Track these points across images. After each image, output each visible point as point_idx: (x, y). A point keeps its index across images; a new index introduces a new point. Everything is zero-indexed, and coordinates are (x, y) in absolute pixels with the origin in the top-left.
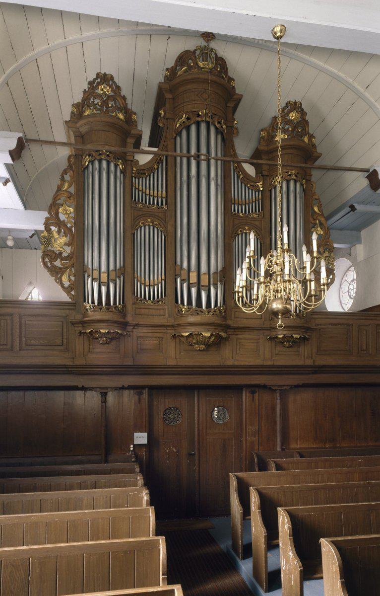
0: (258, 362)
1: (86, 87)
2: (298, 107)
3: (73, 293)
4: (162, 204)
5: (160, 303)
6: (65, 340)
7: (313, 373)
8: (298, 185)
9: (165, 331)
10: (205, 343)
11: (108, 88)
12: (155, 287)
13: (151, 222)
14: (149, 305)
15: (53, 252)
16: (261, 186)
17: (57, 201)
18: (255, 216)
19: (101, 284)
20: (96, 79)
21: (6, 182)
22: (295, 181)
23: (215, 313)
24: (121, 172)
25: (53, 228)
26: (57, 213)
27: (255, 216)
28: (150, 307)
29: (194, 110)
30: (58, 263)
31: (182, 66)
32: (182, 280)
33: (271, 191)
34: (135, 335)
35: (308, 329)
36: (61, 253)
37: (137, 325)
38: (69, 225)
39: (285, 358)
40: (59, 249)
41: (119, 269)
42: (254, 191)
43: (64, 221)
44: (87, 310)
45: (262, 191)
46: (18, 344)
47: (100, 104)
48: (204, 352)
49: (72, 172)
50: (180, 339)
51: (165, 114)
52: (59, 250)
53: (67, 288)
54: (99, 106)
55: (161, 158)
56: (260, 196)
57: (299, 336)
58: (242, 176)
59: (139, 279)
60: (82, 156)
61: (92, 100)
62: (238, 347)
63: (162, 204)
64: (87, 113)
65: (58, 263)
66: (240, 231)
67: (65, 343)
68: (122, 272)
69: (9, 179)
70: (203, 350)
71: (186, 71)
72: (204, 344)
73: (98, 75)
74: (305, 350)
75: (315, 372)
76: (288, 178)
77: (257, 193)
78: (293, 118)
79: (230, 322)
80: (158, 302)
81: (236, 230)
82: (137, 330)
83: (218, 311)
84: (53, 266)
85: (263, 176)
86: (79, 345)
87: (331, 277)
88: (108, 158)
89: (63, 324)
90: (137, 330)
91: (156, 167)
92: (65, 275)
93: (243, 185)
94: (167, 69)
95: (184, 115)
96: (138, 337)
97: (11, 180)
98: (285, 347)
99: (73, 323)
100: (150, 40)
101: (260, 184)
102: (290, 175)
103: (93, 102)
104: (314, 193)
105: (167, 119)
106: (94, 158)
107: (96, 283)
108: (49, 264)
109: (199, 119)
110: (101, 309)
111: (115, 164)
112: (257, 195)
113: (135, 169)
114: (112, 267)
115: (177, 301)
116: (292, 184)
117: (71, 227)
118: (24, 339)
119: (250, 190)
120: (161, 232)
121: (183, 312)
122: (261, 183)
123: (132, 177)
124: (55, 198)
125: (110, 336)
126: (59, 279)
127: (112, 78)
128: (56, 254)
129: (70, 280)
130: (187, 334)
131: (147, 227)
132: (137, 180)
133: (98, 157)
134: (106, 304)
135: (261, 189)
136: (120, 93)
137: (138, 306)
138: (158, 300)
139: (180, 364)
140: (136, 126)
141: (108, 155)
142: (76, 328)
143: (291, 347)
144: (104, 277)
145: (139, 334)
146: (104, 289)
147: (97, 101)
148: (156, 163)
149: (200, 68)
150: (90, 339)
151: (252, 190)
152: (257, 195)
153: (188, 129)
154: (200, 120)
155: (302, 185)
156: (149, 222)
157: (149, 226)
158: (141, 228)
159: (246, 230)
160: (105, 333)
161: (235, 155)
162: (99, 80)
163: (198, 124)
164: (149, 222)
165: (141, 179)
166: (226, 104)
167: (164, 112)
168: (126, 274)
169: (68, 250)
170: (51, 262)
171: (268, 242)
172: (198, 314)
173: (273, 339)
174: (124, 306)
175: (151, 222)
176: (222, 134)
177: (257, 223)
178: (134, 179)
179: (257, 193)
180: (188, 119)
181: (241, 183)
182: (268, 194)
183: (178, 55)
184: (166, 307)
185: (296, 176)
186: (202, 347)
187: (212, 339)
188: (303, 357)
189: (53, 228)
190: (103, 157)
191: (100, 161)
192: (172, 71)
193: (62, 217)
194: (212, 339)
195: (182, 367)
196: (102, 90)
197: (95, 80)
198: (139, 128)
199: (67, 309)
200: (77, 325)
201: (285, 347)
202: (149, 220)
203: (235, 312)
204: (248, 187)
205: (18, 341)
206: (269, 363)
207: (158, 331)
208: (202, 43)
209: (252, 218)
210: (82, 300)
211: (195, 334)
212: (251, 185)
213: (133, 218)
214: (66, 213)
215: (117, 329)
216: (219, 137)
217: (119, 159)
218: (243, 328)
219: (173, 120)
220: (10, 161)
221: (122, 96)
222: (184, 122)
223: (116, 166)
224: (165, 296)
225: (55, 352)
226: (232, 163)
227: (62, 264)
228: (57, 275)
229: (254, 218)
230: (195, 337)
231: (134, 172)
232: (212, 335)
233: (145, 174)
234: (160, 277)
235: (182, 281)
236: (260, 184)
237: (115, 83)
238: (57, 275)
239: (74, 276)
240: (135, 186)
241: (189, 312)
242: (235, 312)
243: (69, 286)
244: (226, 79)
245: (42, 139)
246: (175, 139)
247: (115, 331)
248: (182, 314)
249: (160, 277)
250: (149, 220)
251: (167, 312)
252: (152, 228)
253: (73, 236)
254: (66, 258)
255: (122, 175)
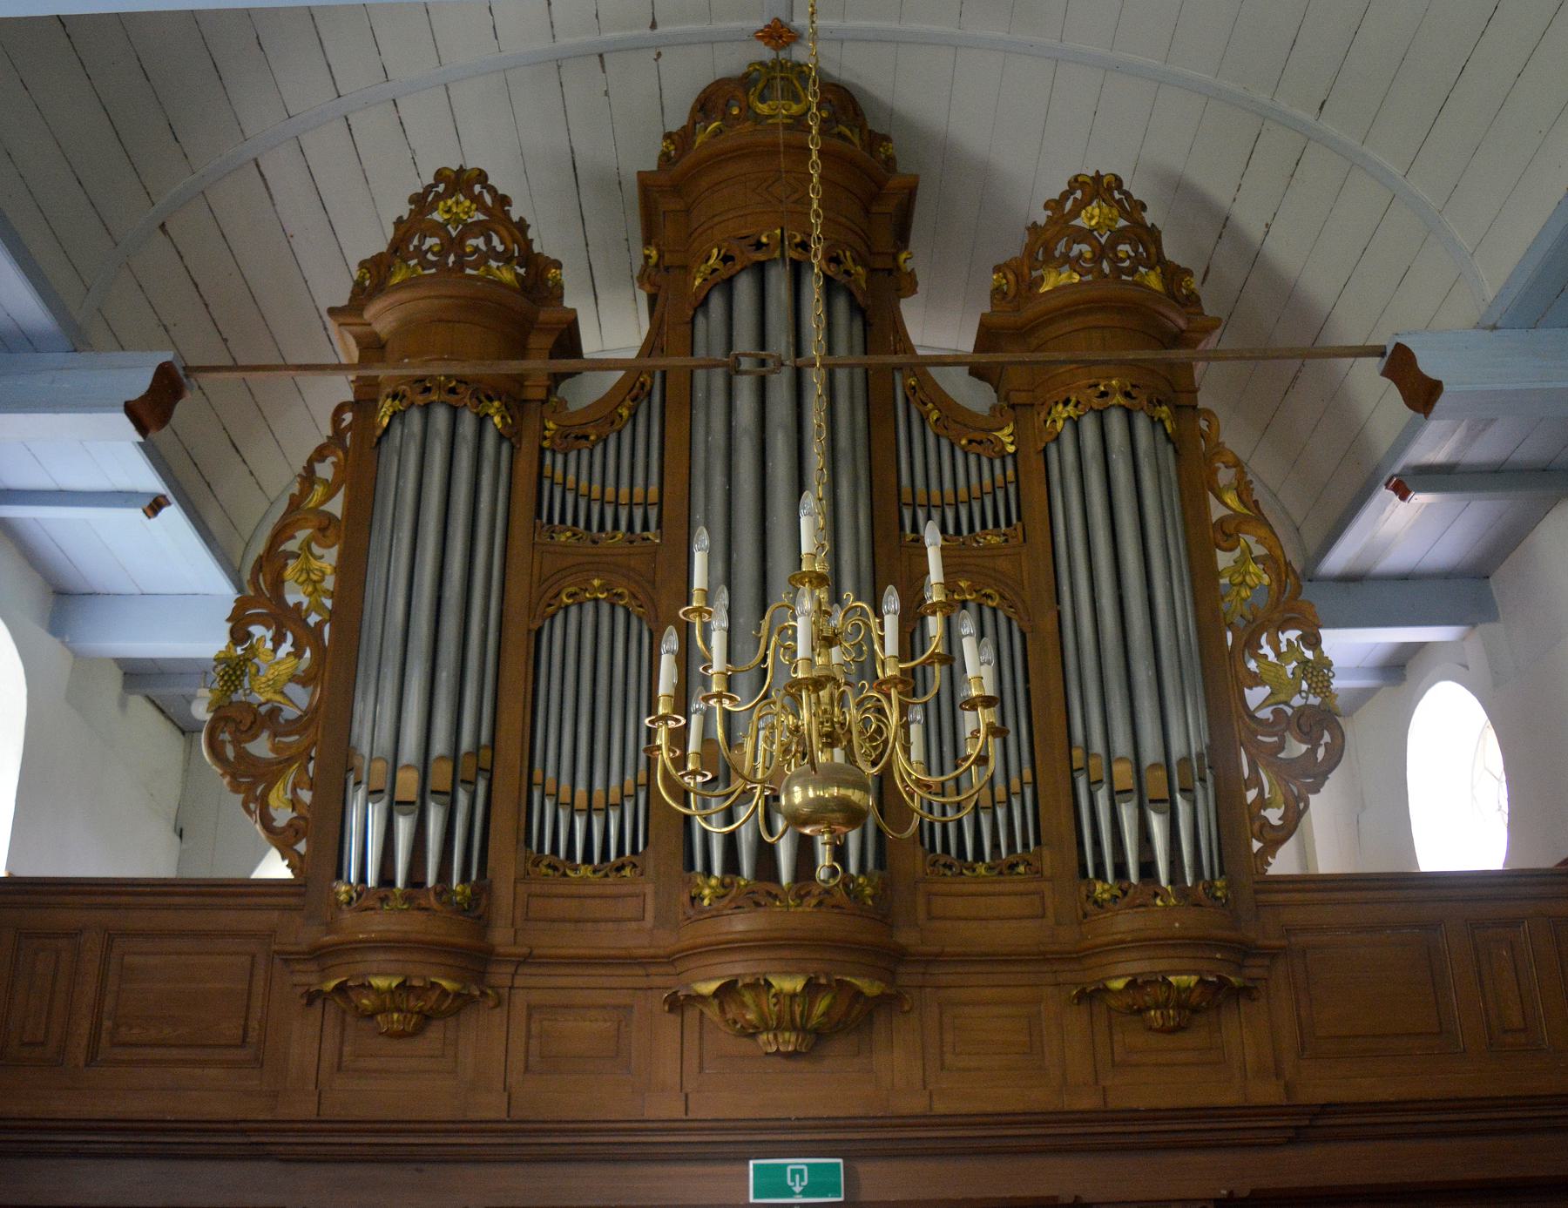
0: (1038, 1097)
1: (404, 210)
2: (1109, 189)
3: (302, 847)
4: (646, 527)
5: (627, 872)
6: (254, 1024)
7: (1291, 1141)
8: (1142, 424)
9: (642, 982)
10: (793, 1020)
11: (467, 203)
12: (595, 818)
13: (602, 589)
14: (584, 881)
15: (248, 706)
16: (1010, 439)
17: (282, 543)
18: (994, 540)
19: (396, 808)
20: (1071, 191)
21: (155, 506)
22: (1129, 414)
23: (829, 901)
24: (501, 437)
25: (257, 630)
26: (278, 584)
27: (994, 540)
28: (587, 890)
29: (744, 232)
30: (261, 747)
31: (708, 119)
32: (1090, 784)
33: (1045, 451)
34: (520, 999)
35: (1242, 951)
36: (275, 712)
37: (527, 960)
38: (313, 619)
39: (1160, 1077)
40: (270, 695)
41: (467, 754)
42: (985, 461)
43: (299, 604)
44: (338, 904)
45: (1014, 455)
46: (84, 1043)
47: (436, 249)
48: (790, 1065)
49: (341, 454)
50: (702, 1013)
51: (661, 256)
52: (268, 702)
53: (283, 830)
54: (434, 254)
55: (643, 385)
56: (1010, 472)
57: (1193, 980)
58: (934, 416)
59: (550, 788)
60: (376, 401)
61: (416, 242)
62: (949, 1037)
63: (646, 527)
64: (396, 280)
65: (261, 747)
66: (570, 596)
67: (253, 1036)
68: (475, 767)
69: (164, 497)
70: (788, 1056)
71: (718, 132)
72: (793, 1028)
73: (440, 175)
74: (1242, 1035)
75: (1297, 1137)
76: (1097, 403)
77: (997, 463)
78: (1093, 222)
79: (906, 937)
80: (620, 869)
81: (551, 593)
82: (532, 982)
83: (840, 894)
84: (243, 755)
85: (1013, 407)
86: (304, 1042)
87: (1327, 738)
88: (452, 399)
89: (253, 965)
90: (532, 982)
91: (625, 413)
92: (280, 785)
93: (945, 443)
94: (668, 136)
95: (715, 251)
96: (531, 1010)
97: (170, 497)
98: (1150, 1029)
99: (288, 958)
100: (603, 67)
101: (1005, 435)
102: (1103, 394)
103: (417, 248)
104: (1218, 444)
105: (667, 269)
106: (405, 402)
107: (377, 806)
108: (230, 752)
109: (760, 256)
110: (383, 900)
111: (477, 414)
112: (998, 471)
113: (551, 425)
114: (440, 746)
115: (690, 865)
116: (1116, 423)
117: (320, 625)
118: (107, 1024)
119: (972, 459)
120: (640, 619)
121: (706, 902)
122: (1008, 431)
123: (542, 450)
124: (282, 533)
125: (415, 1004)
126: (256, 799)
127: (482, 177)
128: (256, 713)
129: (294, 803)
130: (712, 986)
131: (589, 608)
132: (560, 458)
133: (420, 399)
134: (1171, 882)
135: (1011, 449)
136: (507, 213)
137: (536, 888)
138: (1013, 859)
139: (1115, 1103)
140: (561, 296)
141: (452, 391)
142: (297, 979)
143: (1179, 1028)
144: (408, 784)
145: (537, 997)
146: (404, 827)
147: (431, 241)
148: (628, 402)
149: (759, 118)
150: (349, 1019)
151: (979, 456)
152: (998, 471)
153: (728, 285)
154: (763, 258)
155: (1155, 422)
156: (596, 590)
157: (596, 600)
158: (567, 608)
159: (962, 591)
160: (391, 991)
161: (908, 348)
162: (441, 188)
163: (760, 270)
164: (596, 590)
165: (573, 456)
166: (867, 212)
167: (659, 251)
168: (498, 771)
169: (301, 698)
170: (236, 743)
171: (1049, 623)
172: (758, 904)
173: (1092, 996)
174: (482, 890)
175: (602, 589)
176: (851, 296)
177: (1003, 564)
178: (548, 456)
179: (997, 463)
180: (726, 259)
181: (938, 437)
182: (1036, 461)
183: (695, 97)
184: (649, 889)
185: (1127, 395)
186: (789, 1041)
187: (822, 1005)
188: (1242, 1062)
189: (257, 630)
190: (435, 398)
191: (426, 409)
192: (680, 140)
193: (294, 595)
194: (822, 1005)
195: (1133, 1115)
196: (448, 211)
197: (1065, 196)
198: (568, 303)
199: (275, 907)
200: (298, 967)
201: (1150, 1029)
202: (596, 582)
203: (929, 895)
204: (963, 448)
205: (84, 1027)
206: (1087, 1102)
207: (614, 982)
208: (766, 53)
209: (980, 549)
210: (331, 871)
211: (746, 986)
212: (970, 442)
213: (535, 578)
214: (308, 578)
215: (445, 977)
216: (841, 305)
217: (491, 400)
218: (964, 959)
219: (686, 268)
220: (140, 439)
221: (515, 218)
222: (714, 271)
223: (482, 420)
224: (1038, 842)
225: (212, 1072)
226: (898, 377)
227: (274, 749)
228: (251, 788)
229: (989, 547)
230: (748, 998)
231: (547, 433)
232: (812, 987)
233: (586, 437)
234: (629, 778)
235: (1092, 785)
236: (1005, 435)
237: (1128, 195)
238: (251, 788)
239: (312, 786)
240: (552, 478)
241: (726, 900)
242: (929, 895)
243: (290, 825)
244: (856, 140)
245: (291, 361)
246: (693, 321)
247: (433, 984)
248: (703, 911)
249: (629, 778)
250: (596, 582)
251: (1048, 901)
252: (605, 609)
253: (320, 652)
254: (296, 726)
255: (505, 447)
